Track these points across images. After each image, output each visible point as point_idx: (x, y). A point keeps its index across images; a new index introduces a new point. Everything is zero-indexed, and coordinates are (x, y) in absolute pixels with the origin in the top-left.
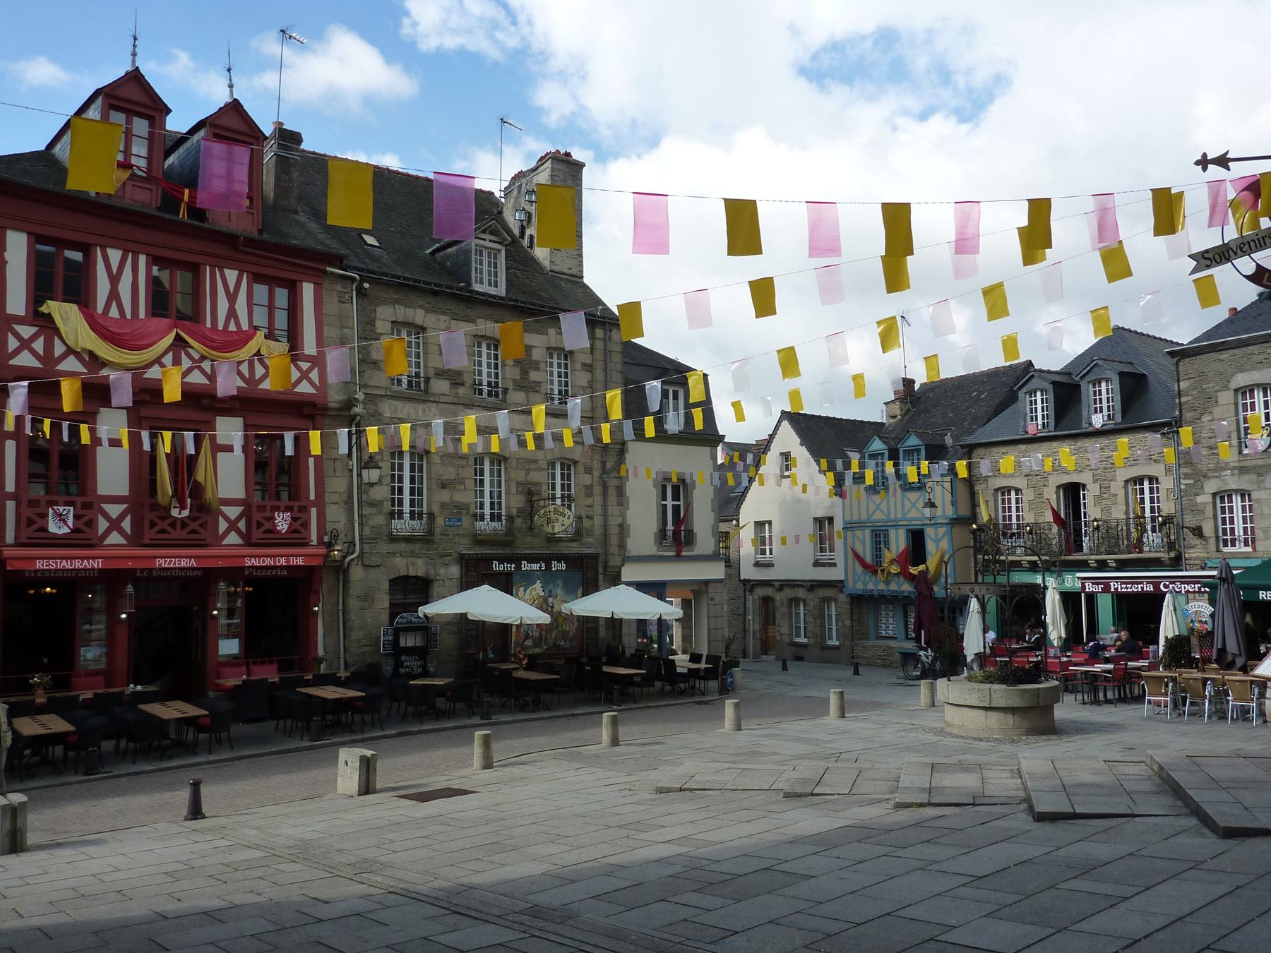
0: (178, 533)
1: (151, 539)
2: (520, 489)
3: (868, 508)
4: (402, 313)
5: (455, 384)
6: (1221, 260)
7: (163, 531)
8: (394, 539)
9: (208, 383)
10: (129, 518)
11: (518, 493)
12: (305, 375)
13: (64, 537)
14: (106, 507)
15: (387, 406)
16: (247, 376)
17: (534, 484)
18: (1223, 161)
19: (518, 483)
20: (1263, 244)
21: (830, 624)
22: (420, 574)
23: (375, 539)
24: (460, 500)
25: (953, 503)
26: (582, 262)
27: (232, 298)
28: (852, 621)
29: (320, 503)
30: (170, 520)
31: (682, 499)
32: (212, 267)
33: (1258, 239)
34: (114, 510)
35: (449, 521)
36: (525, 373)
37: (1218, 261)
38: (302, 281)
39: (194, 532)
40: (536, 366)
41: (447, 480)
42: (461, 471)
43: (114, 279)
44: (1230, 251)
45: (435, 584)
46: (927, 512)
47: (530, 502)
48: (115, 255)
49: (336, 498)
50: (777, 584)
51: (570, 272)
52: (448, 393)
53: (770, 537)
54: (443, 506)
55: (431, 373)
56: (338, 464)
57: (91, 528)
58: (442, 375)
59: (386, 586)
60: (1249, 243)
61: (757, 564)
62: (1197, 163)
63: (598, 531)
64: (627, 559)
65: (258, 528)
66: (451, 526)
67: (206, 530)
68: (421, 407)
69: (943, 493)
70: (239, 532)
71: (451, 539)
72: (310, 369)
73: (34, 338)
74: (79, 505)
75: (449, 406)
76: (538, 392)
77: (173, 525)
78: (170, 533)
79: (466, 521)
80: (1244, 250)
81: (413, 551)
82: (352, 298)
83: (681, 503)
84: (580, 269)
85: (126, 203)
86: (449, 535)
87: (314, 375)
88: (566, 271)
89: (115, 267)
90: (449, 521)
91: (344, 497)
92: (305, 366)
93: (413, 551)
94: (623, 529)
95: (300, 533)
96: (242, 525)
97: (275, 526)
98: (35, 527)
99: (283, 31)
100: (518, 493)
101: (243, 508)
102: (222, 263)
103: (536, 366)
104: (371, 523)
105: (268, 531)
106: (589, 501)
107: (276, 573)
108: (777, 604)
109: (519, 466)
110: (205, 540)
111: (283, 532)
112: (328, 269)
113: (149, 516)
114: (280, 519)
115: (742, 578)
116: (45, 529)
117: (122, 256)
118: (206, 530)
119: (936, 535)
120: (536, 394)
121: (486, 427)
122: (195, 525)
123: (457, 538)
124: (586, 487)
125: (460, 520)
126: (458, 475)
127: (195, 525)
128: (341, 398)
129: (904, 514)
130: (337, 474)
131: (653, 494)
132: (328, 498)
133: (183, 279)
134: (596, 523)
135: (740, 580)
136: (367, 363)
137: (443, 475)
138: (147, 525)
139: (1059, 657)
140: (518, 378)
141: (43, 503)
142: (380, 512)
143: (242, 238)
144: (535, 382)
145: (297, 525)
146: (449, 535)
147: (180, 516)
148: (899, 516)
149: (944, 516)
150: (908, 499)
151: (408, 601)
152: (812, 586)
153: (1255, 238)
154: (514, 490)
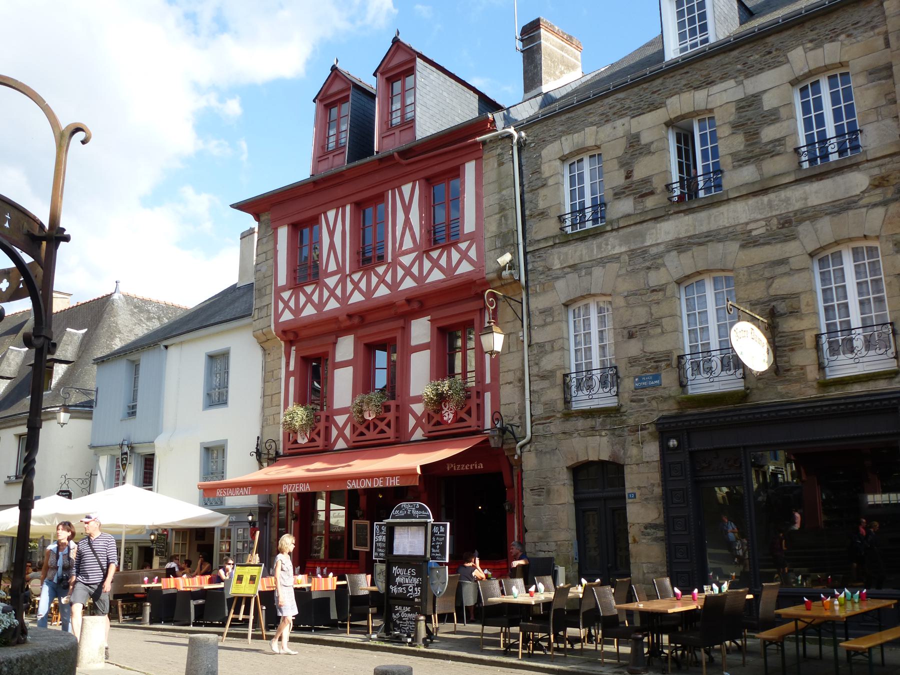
4: (567, 144)
15: (556, 257)
17: (783, 298)
22: (605, 457)
23: (549, 418)
24: (656, 350)
31: (882, 273)
32: (393, 189)
35: (640, 380)
36: (752, 136)
41: (635, 327)
42: (654, 309)
45: (627, 470)
58: (624, 193)
65: (390, 421)
66: (643, 388)
71: (645, 405)
75: (633, 228)
78: (358, 436)
82: (512, 154)
85: (323, 174)
86: (642, 400)
90: (640, 380)
91: (518, 374)
93: (593, 428)
104: (543, 399)
105: (438, 423)
107: (474, 467)
109: (754, 277)
110: (470, 427)
111: (449, 422)
116: (296, 442)
120: (777, 158)
121: (689, 237)
123: (654, 403)
125: (656, 377)
126: (652, 315)
130: (511, 350)
136: (534, 217)
137: (630, 320)
142: (553, 386)
143: (396, 154)
144: (771, 142)
146: (642, 400)
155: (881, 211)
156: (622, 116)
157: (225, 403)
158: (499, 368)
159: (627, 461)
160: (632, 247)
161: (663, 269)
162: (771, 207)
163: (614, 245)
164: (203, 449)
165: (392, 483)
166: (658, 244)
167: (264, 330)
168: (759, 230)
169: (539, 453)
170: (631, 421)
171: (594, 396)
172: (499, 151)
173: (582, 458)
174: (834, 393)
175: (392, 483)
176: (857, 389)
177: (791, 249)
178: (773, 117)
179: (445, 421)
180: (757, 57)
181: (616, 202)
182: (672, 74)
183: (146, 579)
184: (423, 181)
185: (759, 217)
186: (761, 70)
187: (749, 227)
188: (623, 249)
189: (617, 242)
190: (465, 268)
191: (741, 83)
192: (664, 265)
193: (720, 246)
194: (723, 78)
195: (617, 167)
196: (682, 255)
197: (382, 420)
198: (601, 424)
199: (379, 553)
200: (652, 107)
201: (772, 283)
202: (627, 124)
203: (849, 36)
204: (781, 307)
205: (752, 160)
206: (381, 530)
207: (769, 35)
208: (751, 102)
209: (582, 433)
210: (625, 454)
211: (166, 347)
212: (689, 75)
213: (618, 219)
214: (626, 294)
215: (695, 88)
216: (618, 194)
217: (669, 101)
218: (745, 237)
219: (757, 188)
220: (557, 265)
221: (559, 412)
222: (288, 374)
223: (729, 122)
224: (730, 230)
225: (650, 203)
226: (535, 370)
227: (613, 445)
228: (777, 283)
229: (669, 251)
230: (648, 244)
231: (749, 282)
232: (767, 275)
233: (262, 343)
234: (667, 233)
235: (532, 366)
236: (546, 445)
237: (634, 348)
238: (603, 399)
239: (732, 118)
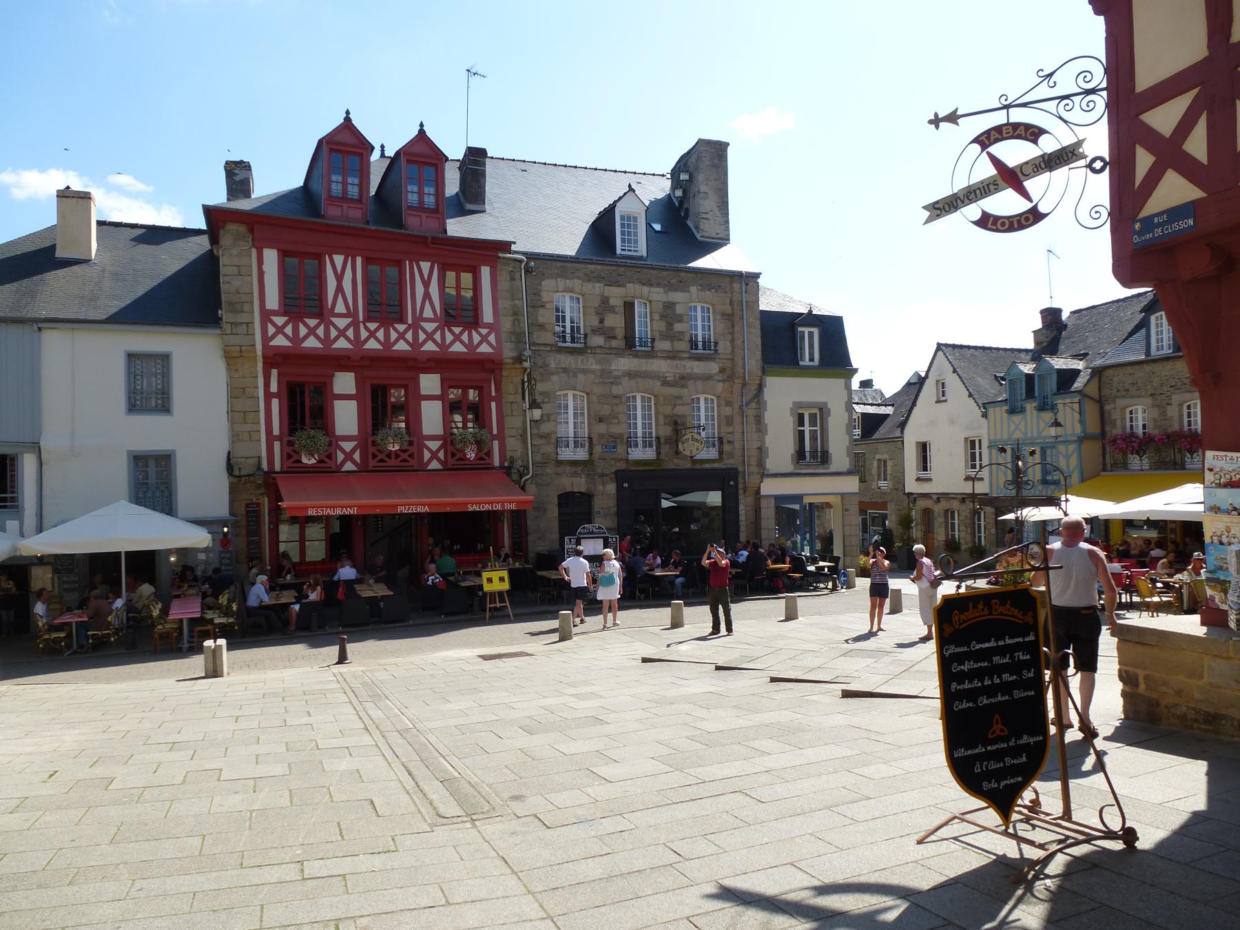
0: (392, 462)
1: (289, 467)
2: (667, 421)
3: (1009, 427)
5: (608, 337)
6: (950, 209)
7: (382, 461)
8: (560, 463)
9: (410, 349)
10: (358, 451)
11: (665, 424)
12: (484, 339)
13: (312, 466)
14: (427, 443)
16: (440, 342)
17: (679, 416)
18: (953, 118)
19: (666, 416)
20: (987, 191)
21: (980, 532)
22: (583, 490)
25: (1082, 422)
26: (728, 227)
27: (426, 284)
28: (997, 529)
29: (501, 437)
33: (983, 187)
34: (434, 445)
35: (606, 448)
36: (670, 325)
37: (947, 209)
38: (480, 266)
39: (405, 460)
41: (603, 416)
43: (339, 278)
44: (958, 200)
45: (596, 498)
46: (1053, 431)
47: (676, 431)
48: (339, 259)
49: (513, 432)
50: (935, 497)
51: (718, 236)
52: (603, 345)
53: (980, 453)
54: (601, 436)
55: (589, 331)
56: (515, 406)
57: (489, 457)
58: (597, 331)
59: (556, 500)
60: (975, 191)
61: (918, 479)
62: (930, 122)
63: (738, 453)
64: (764, 475)
67: (413, 459)
68: (580, 358)
69: (1073, 414)
70: (439, 460)
71: (608, 462)
72: (489, 334)
73: (285, 325)
76: (681, 340)
77: (389, 455)
79: (620, 449)
80: (970, 197)
81: (576, 472)
83: (818, 428)
84: (727, 232)
87: (492, 338)
88: (714, 236)
89: (339, 268)
90: (606, 448)
91: (520, 431)
92: (484, 331)
93: (576, 472)
94: (762, 451)
96: (441, 455)
97: (465, 455)
98: (377, 459)
99: (468, 70)
100: (665, 424)
101: (441, 442)
102: (417, 258)
105: (460, 459)
106: (730, 429)
108: (935, 514)
112: (500, 255)
113: (371, 449)
115: (906, 492)
117: (344, 259)
118: (413, 459)
119: (1067, 450)
120: (680, 342)
121: (636, 371)
122: (405, 456)
124: (727, 417)
125: (615, 447)
126: (613, 411)
127: (405, 456)
128: (514, 354)
129: (1039, 433)
131: (789, 423)
132: (507, 432)
133: (392, 271)
134: (736, 447)
135: (905, 494)
136: (535, 326)
140: (664, 329)
147: (393, 449)
148: (1035, 435)
149: (1073, 435)
150: (1013, 422)
152: (963, 499)
153: (981, 186)
154: (662, 421)
155: (721, 384)
157: (133, 408)
158: (504, 425)
159: (596, 493)
160: (604, 368)
163: (592, 364)
164: (132, 458)
165: (510, 507)
166: (618, 370)
167: (243, 348)
169: (538, 485)
170: (599, 471)
172: (511, 269)
174: (698, 467)
175: (510, 507)
176: (707, 466)
179: (468, 459)
181: (593, 336)
183: (826, 570)
185: (671, 371)
187: (666, 375)
188: (598, 367)
189: (594, 362)
190: (485, 348)
191: (666, 292)
193: (651, 381)
194: (658, 285)
195: (594, 314)
198: (581, 471)
202: (602, 288)
203: (716, 291)
206: (570, 541)
208: (669, 306)
209: (569, 475)
210: (595, 489)
211: (40, 329)
213: (595, 347)
214: (598, 395)
215: (642, 284)
216: (594, 331)
217: (628, 285)
218: (664, 379)
219: (671, 355)
220: (553, 365)
221: (553, 460)
222: (268, 396)
223: (659, 313)
225: (614, 343)
226: (535, 431)
227: (588, 484)
228: (677, 408)
229: (624, 376)
230: (613, 368)
232: (673, 403)
233: (229, 358)
234: (624, 365)
235: (908, 497)
237: (602, 428)
238: (582, 454)
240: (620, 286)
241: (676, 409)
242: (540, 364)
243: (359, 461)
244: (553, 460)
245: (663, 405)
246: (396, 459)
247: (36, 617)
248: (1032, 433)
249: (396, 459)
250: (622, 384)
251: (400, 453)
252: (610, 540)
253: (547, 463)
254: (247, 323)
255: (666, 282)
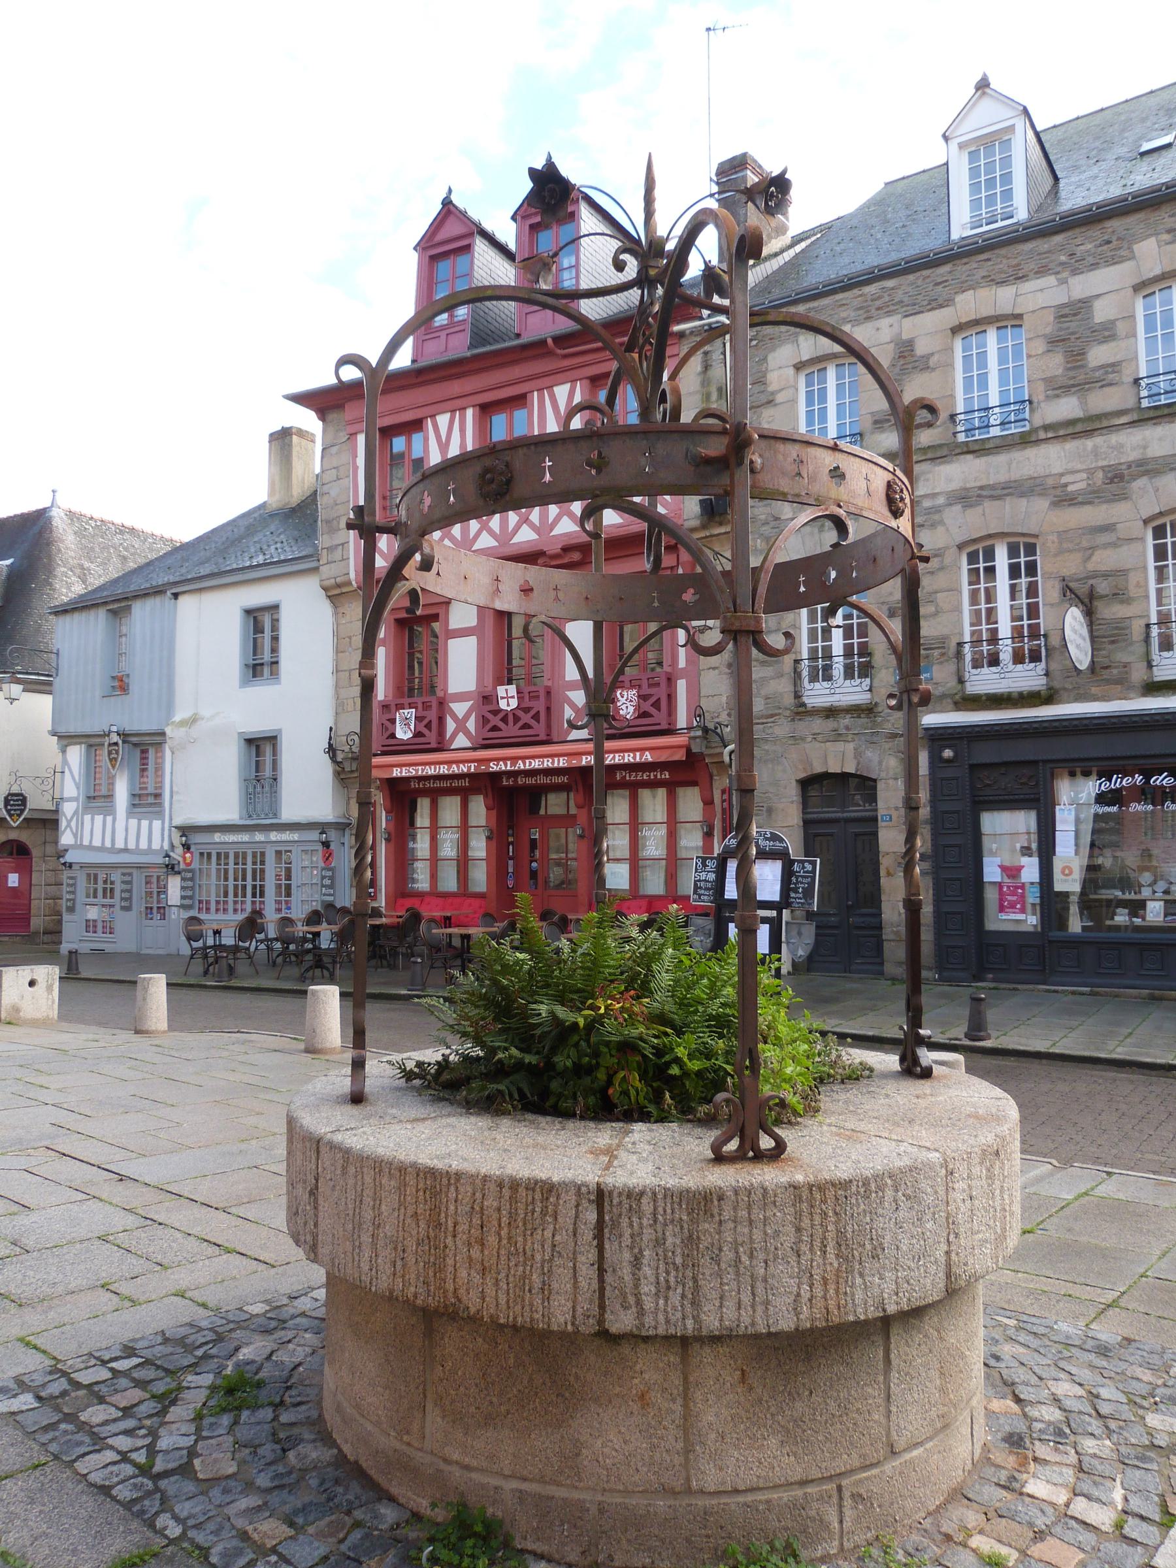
0: (511, 730)
17: (1106, 575)
23: (772, 716)
30: (501, 715)
36: (1076, 358)
39: (526, 726)
40: (1107, 333)
74: (420, 706)
77: (505, 720)
95: (651, 716)
97: (617, 709)
98: (520, 724)
103: (1107, 333)
114: (623, 700)
116: (393, 736)
121: (981, 488)
127: (526, 718)
137: (891, 594)
138: (434, 725)
139: (773, 1549)
141: (393, 708)
145: (647, 706)
151: (845, 815)
156: (889, 313)
161: (940, 529)
162: (1096, 455)
164: (243, 742)
168: (1077, 484)
171: (838, 691)
173: (819, 769)
177: (1118, 512)
178: (1107, 334)
180: (1089, 246)
182: (965, 260)
184: (586, 382)
185: (1079, 467)
186: (1094, 266)
187: (1064, 480)
191: (1063, 282)
192: (941, 522)
196: (969, 511)
197: (527, 710)
199: (700, 895)
200: (934, 304)
201: (1092, 554)
202: (896, 325)
204: (1103, 587)
205: (1073, 390)
206: (704, 865)
207: (1109, 218)
212: (990, 263)
217: (959, 298)
221: (786, 709)
223: (1044, 336)
224: (1038, 481)
231: (1060, 552)
232: (1085, 544)
236: (767, 751)
239: (1048, 330)
240: (941, 306)
241: (1094, 558)
242: (763, 517)
243: (566, 706)
244: (786, 709)
245: (1056, 555)
246: (507, 724)
247: (412, 984)
248: (93, 820)
249: (507, 724)
250: (944, 524)
251: (520, 713)
252: (796, 867)
253: (776, 715)
254: (343, 544)
255: (1063, 258)
